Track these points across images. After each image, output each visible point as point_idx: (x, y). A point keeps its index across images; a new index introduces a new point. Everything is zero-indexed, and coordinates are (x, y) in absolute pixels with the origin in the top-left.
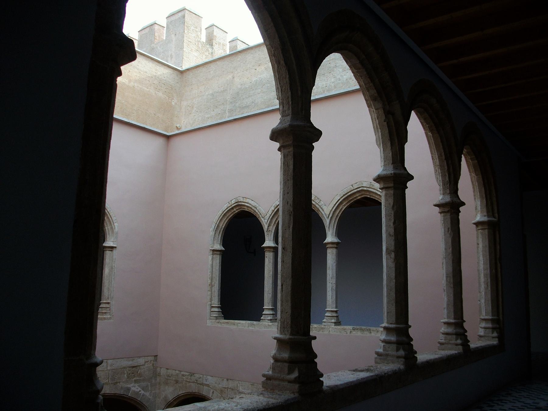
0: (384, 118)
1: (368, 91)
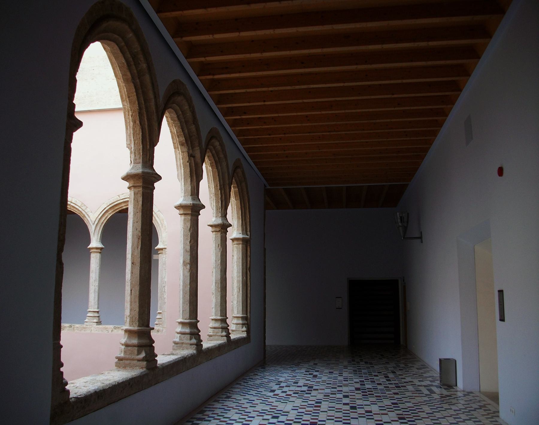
0: (187, 159)
1: (178, 138)
